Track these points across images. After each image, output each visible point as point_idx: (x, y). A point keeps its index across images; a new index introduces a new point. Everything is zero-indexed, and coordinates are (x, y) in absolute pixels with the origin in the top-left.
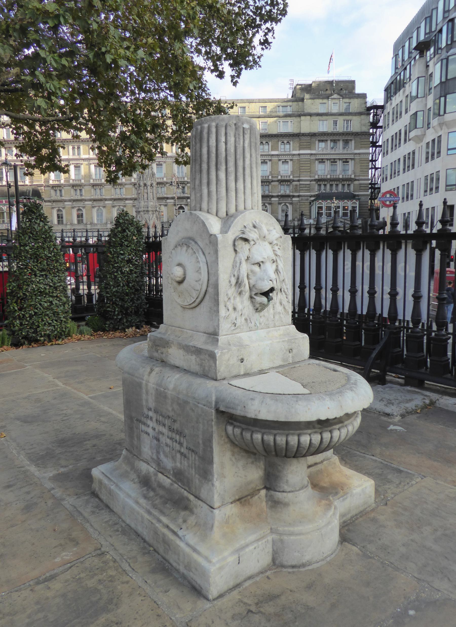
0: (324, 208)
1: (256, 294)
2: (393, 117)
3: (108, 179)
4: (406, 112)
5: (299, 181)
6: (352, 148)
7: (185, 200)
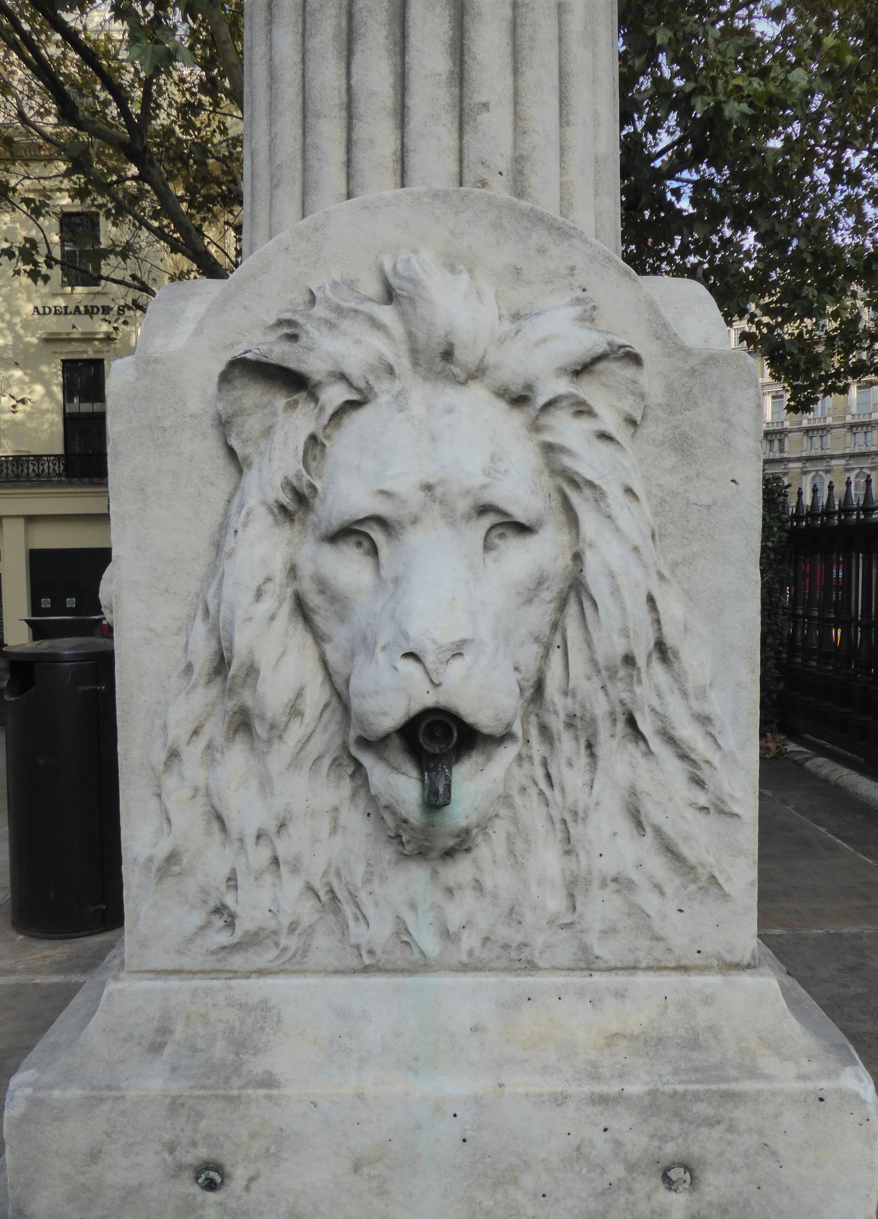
3: (792, 403)
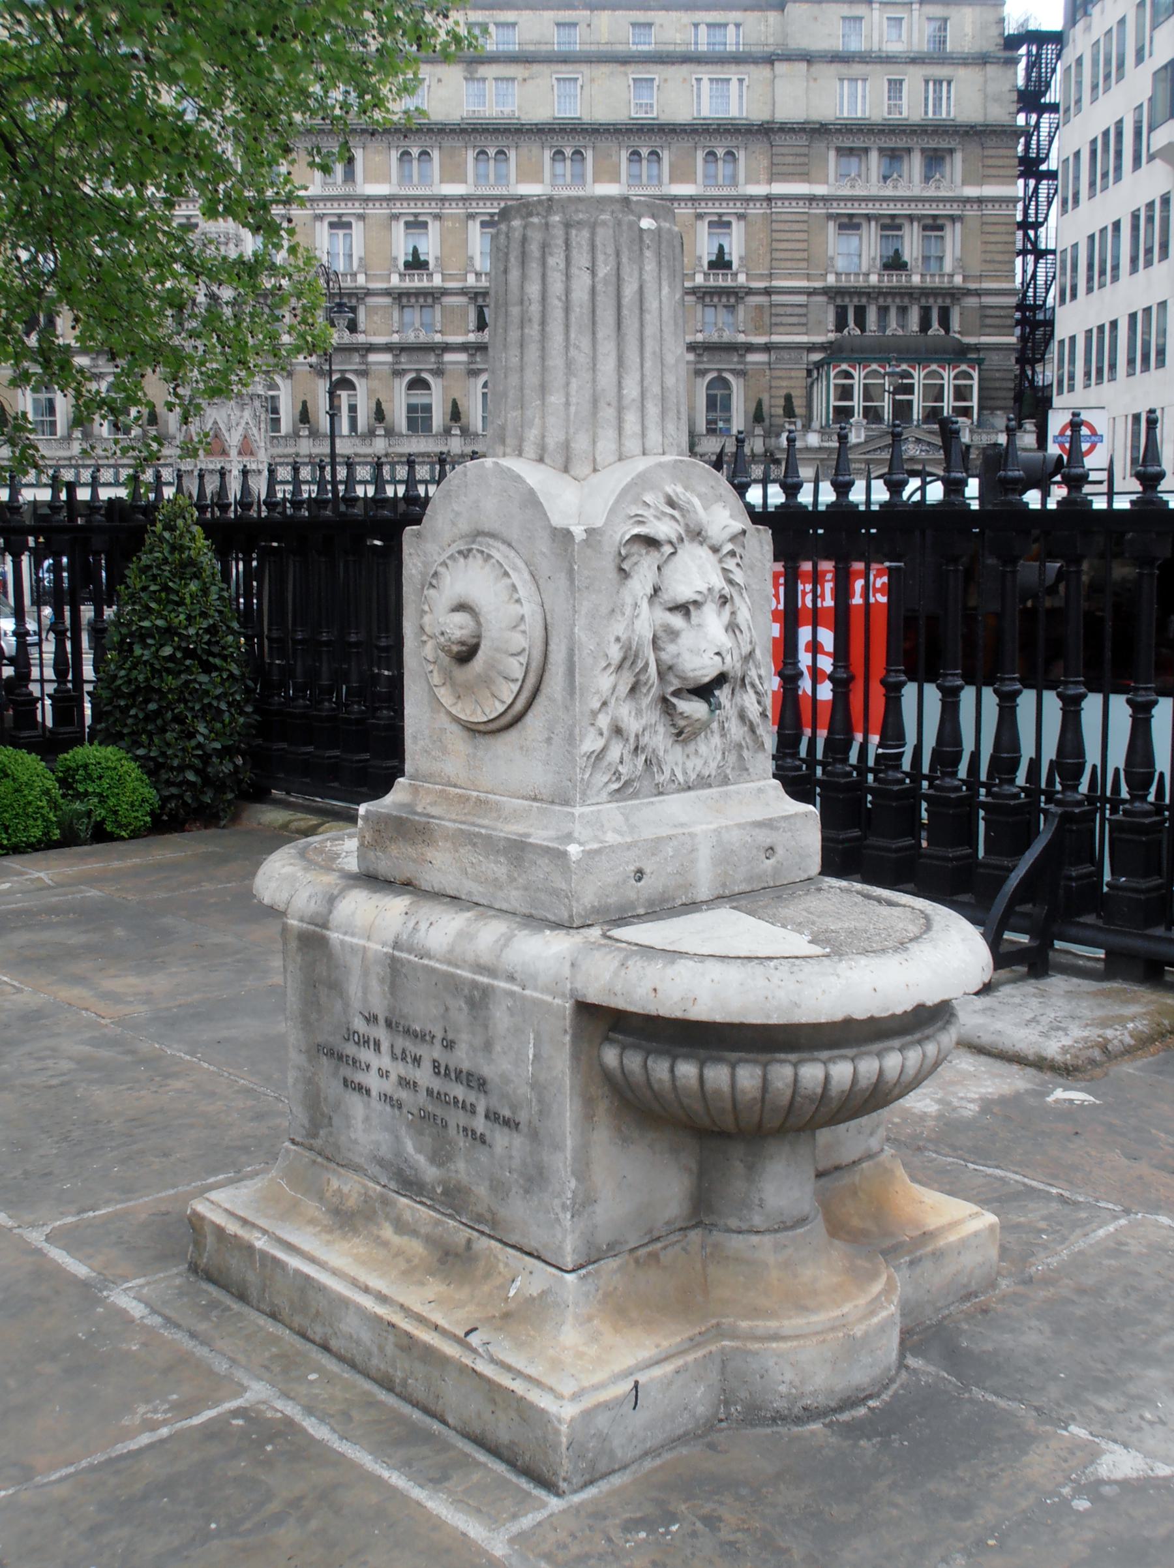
0: (858, 393)
1: (677, 693)
2: (1095, 75)
4: (1140, 58)
5: (768, 292)
6: (957, 181)
7: (356, 358)
